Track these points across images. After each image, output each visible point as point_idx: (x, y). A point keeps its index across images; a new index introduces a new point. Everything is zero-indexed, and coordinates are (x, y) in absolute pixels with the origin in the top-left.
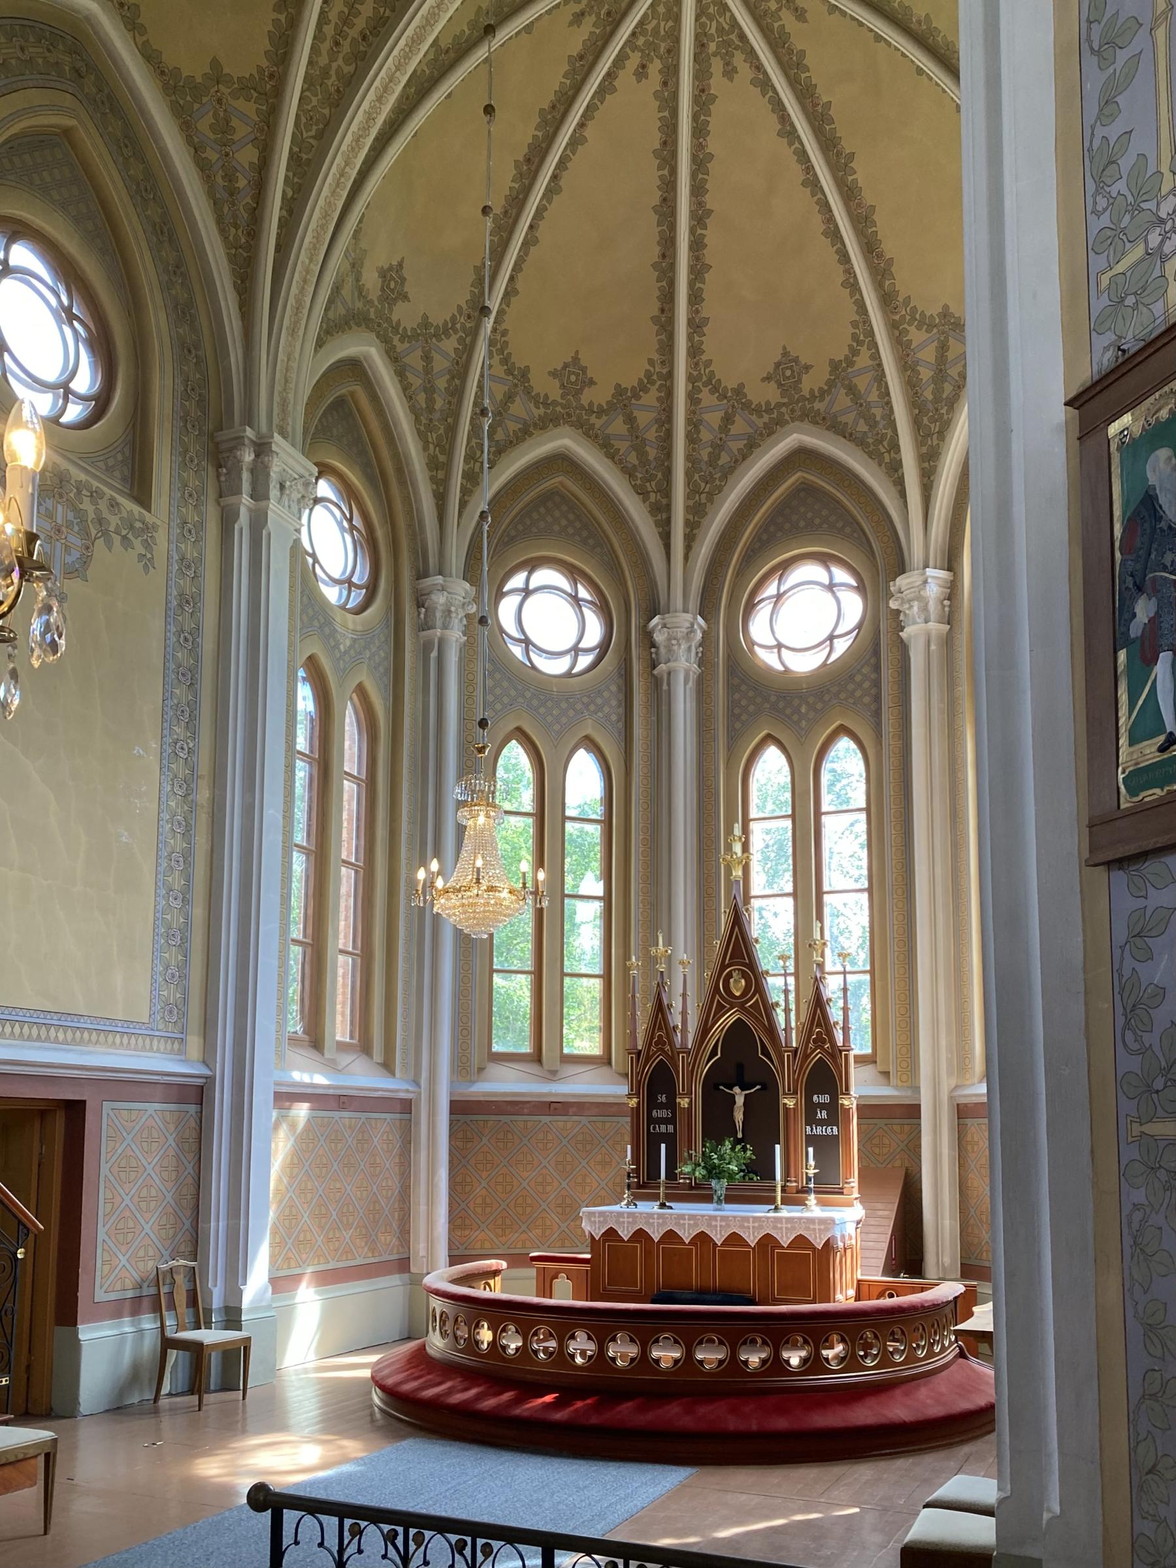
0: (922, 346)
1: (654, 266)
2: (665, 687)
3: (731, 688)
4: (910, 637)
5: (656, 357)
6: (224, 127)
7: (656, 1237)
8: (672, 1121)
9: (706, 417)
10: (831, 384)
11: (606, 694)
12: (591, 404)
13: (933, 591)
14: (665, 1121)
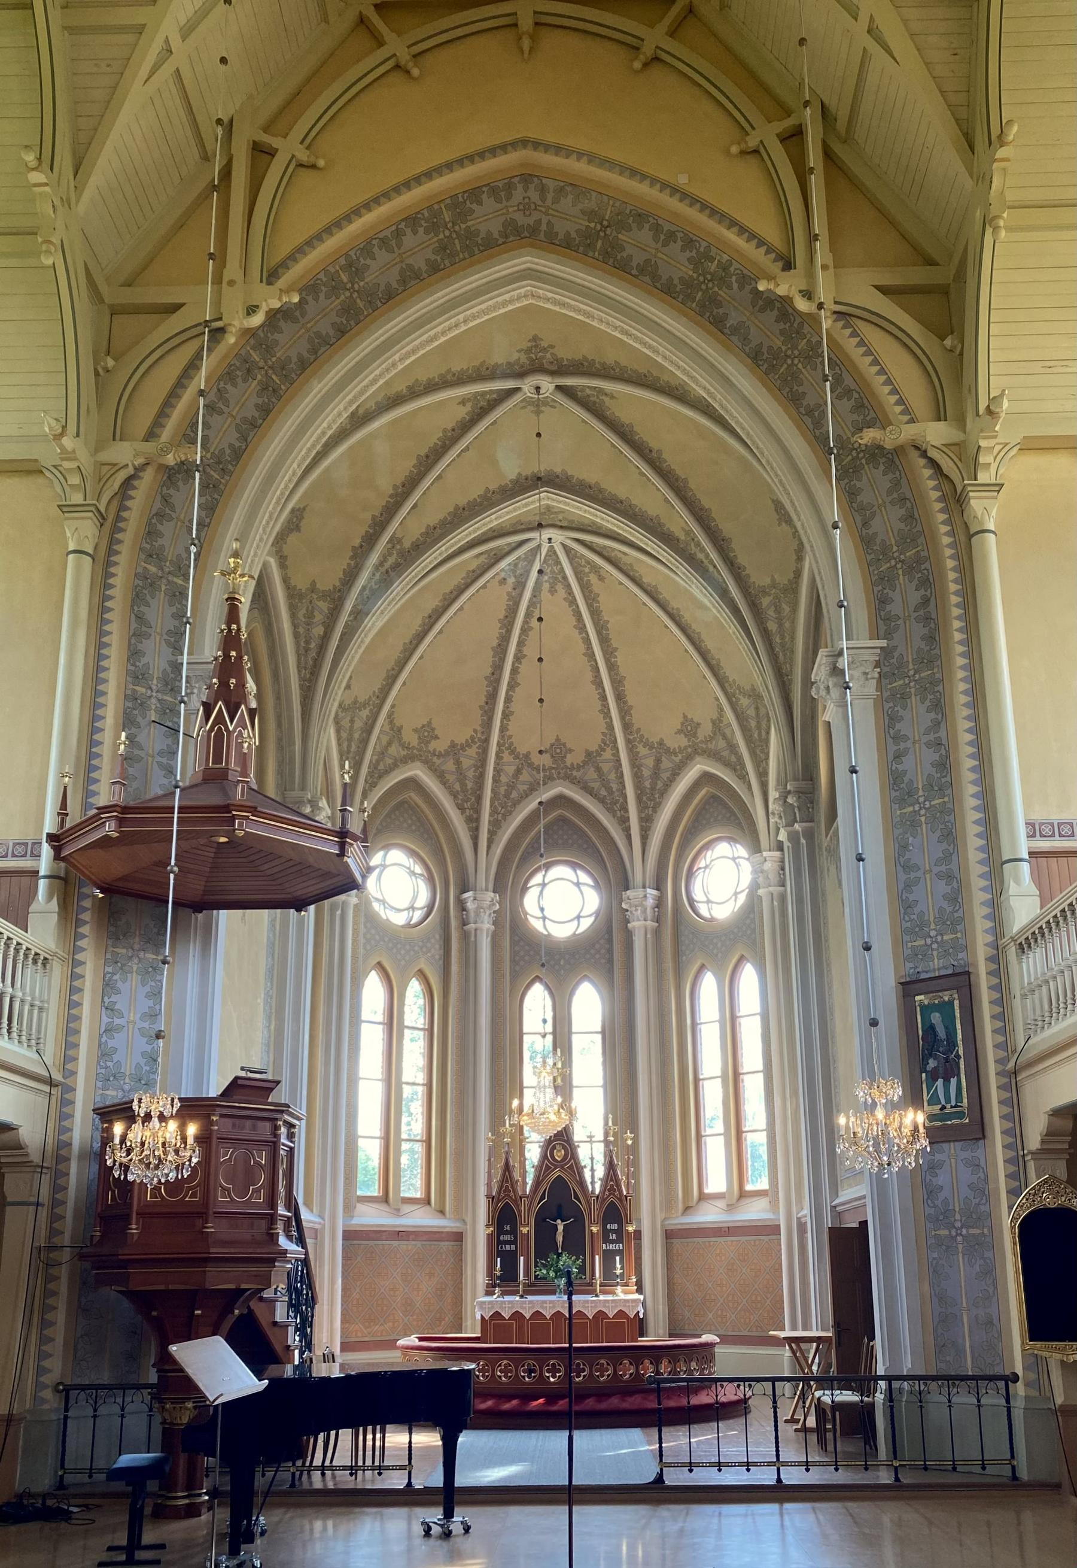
0: (646, 757)
1: (486, 678)
2: (473, 939)
3: (513, 943)
4: (634, 927)
5: (479, 728)
6: (310, 615)
7: (528, 1316)
8: (515, 1242)
9: (506, 768)
10: (585, 763)
11: (433, 941)
12: (435, 750)
13: (650, 902)
14: (509, 1243)
